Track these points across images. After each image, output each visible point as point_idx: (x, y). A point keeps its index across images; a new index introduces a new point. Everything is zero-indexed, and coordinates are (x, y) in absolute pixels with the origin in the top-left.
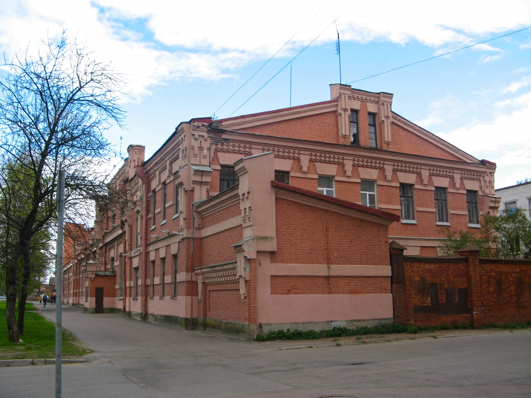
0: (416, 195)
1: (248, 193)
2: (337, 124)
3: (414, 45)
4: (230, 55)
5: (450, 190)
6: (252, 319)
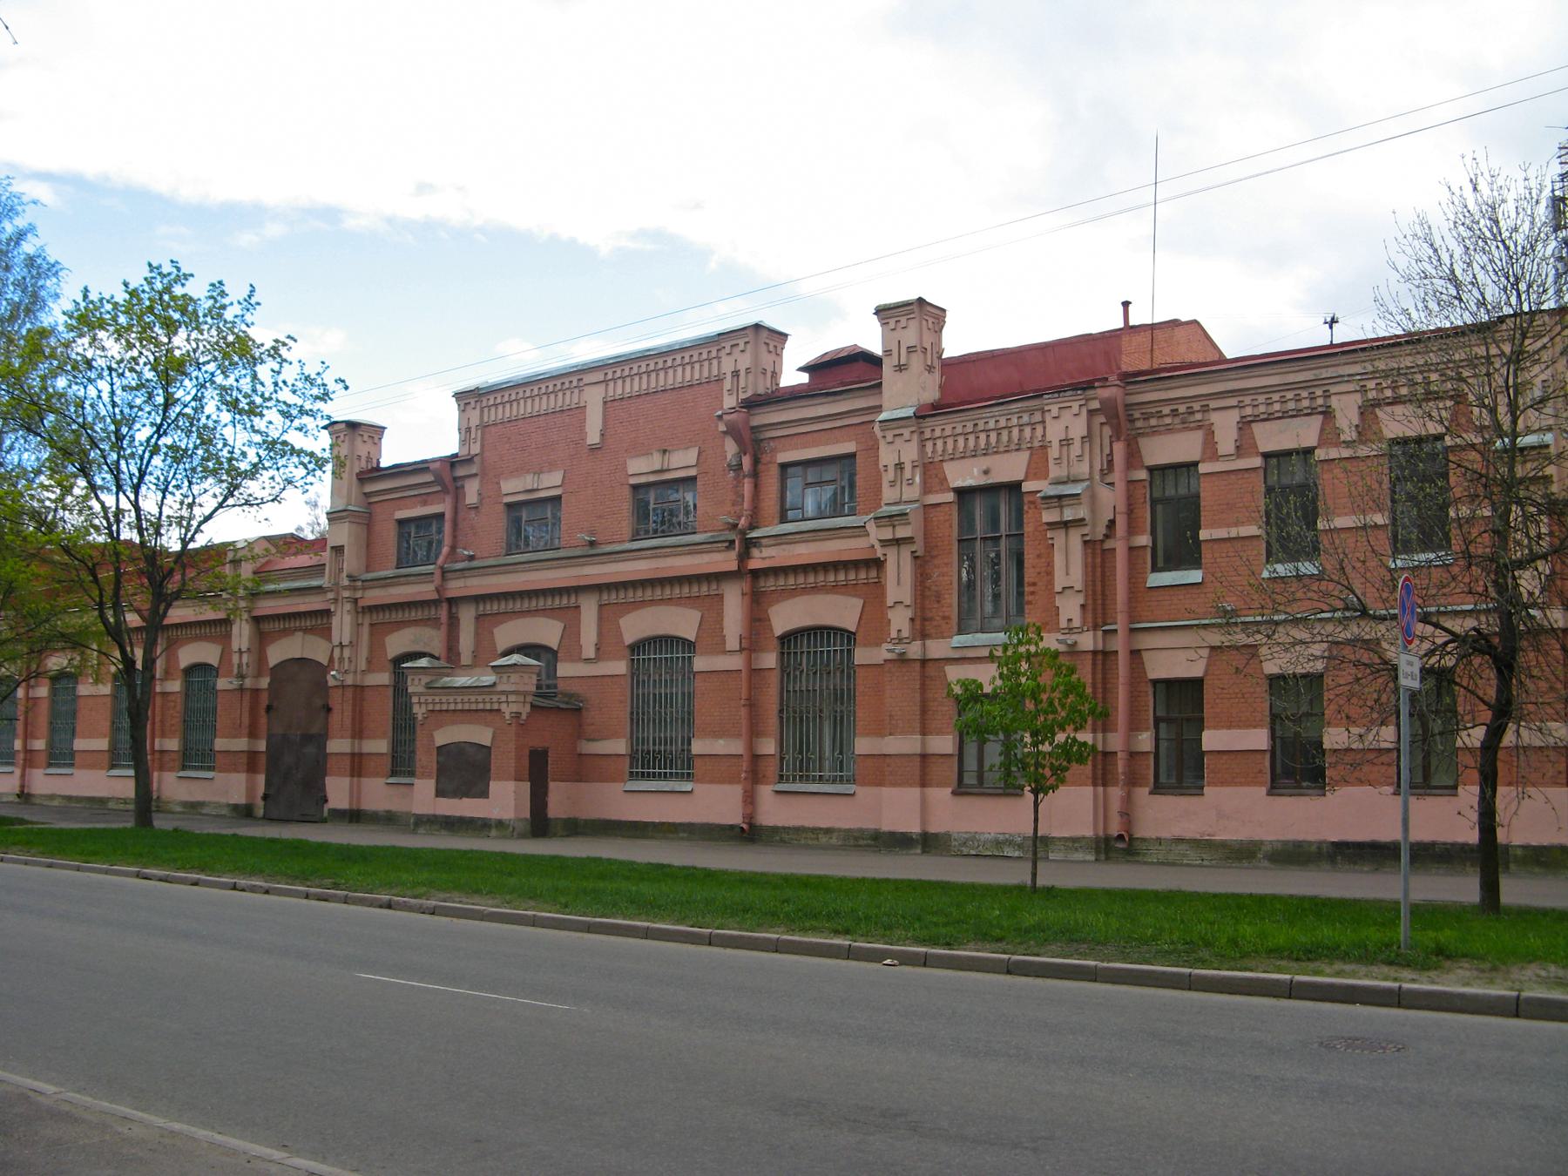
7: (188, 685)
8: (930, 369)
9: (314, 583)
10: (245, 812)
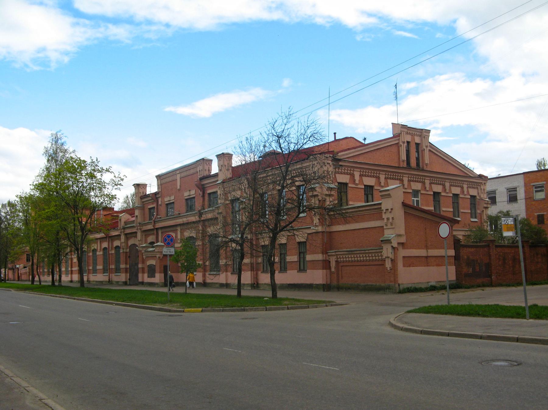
0: (442, 199)
1: (392, 209)
2: (399, 152)
3: (337, 29)
4: (154, 28)
5: (461, 196)
6: (395, 281)
7: (116, 250)
8: (228, 170)
9: (132, 225)
10: (125, 283)
